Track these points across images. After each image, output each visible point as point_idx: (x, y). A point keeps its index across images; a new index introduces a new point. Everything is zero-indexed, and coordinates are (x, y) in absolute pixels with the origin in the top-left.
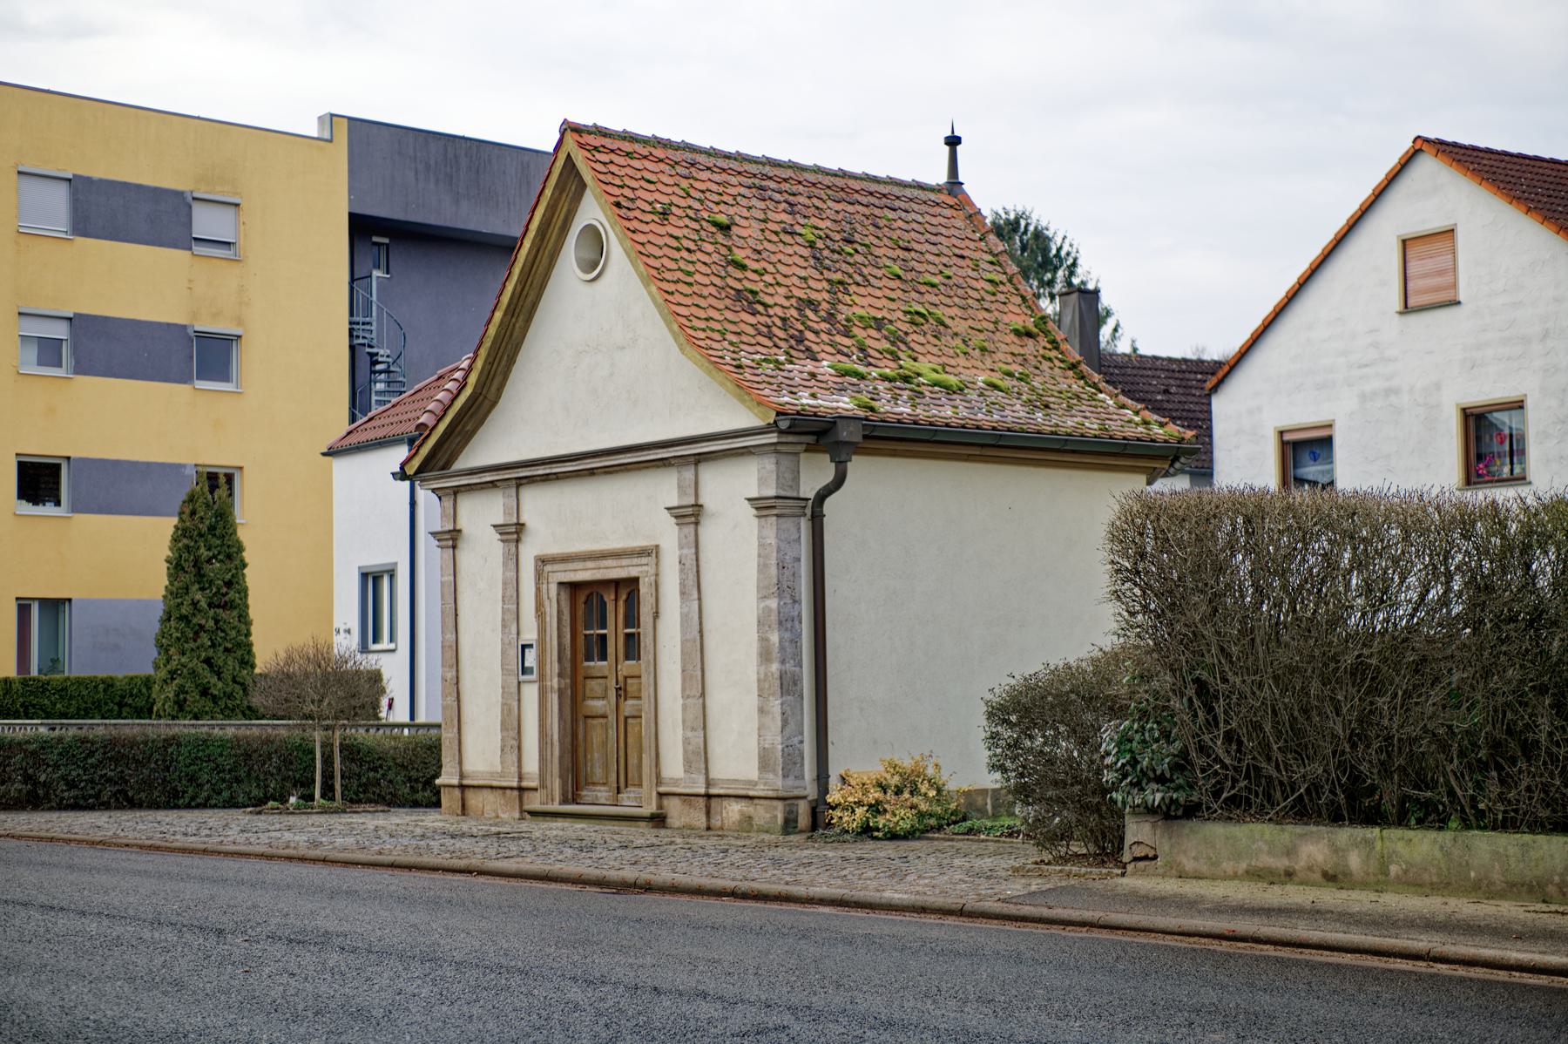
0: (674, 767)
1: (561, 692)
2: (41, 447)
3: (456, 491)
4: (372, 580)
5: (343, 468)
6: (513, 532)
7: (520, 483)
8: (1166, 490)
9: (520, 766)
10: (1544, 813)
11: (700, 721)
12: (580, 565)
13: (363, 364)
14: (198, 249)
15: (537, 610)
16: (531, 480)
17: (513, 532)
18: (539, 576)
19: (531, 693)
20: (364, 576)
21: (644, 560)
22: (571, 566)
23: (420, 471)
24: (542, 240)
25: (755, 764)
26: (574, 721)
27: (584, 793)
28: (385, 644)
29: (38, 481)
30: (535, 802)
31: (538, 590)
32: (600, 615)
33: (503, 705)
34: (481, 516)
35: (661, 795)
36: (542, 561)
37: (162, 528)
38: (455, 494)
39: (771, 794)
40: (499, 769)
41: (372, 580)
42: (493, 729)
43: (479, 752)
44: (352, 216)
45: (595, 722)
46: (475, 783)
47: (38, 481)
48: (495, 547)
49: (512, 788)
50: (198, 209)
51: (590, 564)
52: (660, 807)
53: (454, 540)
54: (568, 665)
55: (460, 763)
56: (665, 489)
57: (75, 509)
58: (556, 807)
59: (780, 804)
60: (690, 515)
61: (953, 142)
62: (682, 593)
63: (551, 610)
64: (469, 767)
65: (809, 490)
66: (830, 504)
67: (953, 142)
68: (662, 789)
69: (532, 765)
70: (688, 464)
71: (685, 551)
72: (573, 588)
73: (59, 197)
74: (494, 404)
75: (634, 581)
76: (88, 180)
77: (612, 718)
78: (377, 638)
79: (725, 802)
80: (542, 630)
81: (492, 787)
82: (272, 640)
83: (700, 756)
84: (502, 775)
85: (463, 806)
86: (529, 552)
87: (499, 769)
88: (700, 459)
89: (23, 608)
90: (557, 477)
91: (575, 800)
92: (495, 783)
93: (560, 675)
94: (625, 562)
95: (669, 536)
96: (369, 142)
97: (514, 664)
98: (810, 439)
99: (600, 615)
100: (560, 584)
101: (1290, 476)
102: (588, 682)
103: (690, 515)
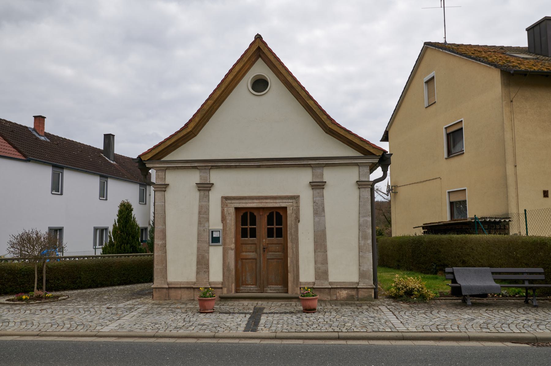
6: (205, 188)
12: (250, 201)
16: (213, 167)
17: (205, 188)
21: (290, 201)
27: (241, 288)
45: (247, 261)
51: (256, 201)
56: (306, 176)
58: (233, 294)
60: (318, 186)
69: (216, 275)
83: (322, 272)
84: (195, 283)
86: (215, 198)
90: (236, 167)
94: (277, 201)
103: (318, 186)
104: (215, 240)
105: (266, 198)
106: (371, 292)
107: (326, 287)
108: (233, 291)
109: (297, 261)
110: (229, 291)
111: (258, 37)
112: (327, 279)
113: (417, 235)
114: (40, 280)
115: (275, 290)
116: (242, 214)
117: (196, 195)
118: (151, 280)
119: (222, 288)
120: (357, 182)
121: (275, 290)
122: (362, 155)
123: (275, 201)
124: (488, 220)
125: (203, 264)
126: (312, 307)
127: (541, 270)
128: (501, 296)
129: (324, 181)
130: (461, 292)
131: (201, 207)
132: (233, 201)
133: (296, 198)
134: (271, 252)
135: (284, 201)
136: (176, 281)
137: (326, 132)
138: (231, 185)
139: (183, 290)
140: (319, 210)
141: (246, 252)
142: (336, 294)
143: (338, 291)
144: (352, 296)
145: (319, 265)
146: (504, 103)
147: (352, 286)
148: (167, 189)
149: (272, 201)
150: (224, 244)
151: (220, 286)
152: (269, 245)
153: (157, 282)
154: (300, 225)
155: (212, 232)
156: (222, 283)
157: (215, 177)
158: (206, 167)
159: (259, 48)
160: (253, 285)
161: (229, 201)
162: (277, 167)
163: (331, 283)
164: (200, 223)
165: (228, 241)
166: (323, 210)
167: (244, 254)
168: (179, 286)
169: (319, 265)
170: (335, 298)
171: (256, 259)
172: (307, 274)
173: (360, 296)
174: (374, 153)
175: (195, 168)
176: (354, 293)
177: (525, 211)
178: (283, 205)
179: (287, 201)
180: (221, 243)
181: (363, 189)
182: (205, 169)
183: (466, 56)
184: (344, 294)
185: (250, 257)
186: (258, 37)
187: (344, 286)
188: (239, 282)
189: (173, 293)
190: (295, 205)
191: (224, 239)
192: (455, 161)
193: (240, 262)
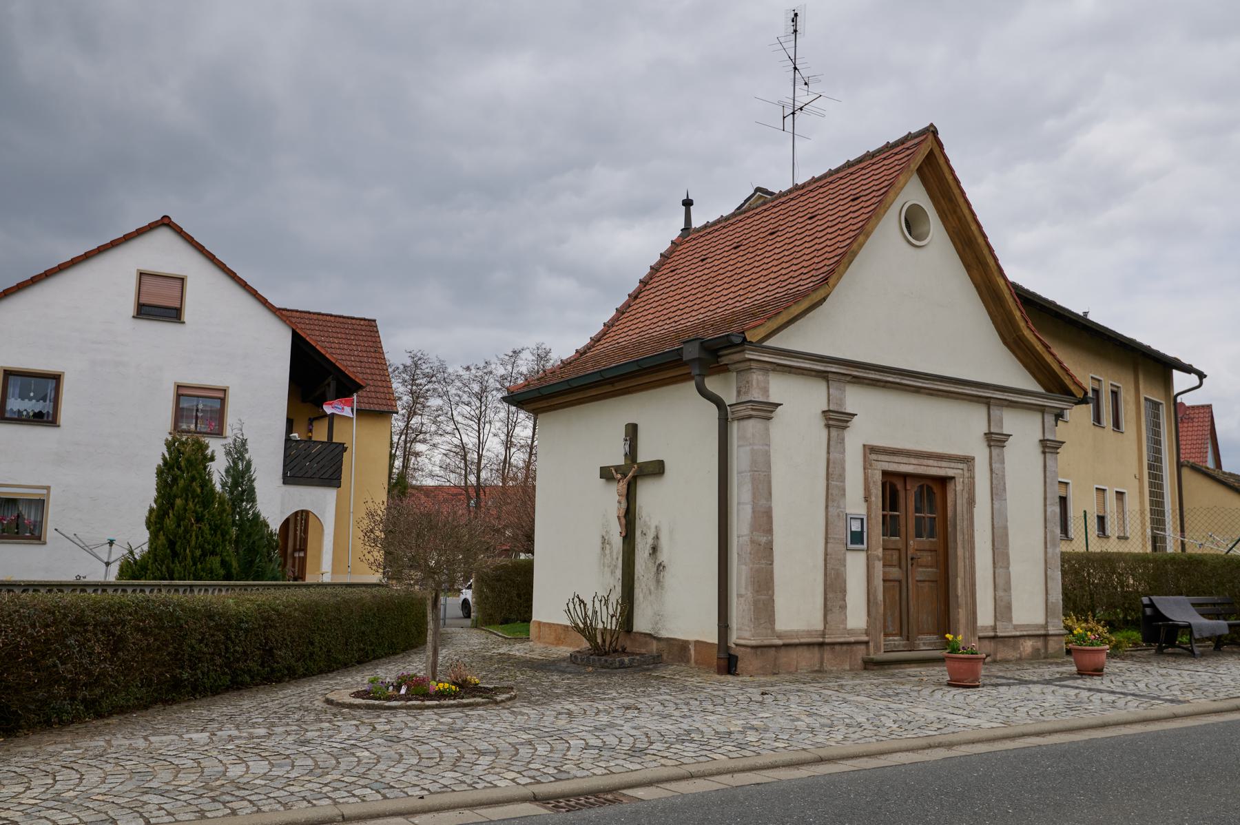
0: (985, 617)
6: (837, 420)
8: (783, 778)
10: (1221, 626)
11: (1002, 585)
12: (905, 460)
16: (857, 381)
17: (837, 420)
21: (961, 466)
22: (896, 459)
51: (913, 461)
59: (735, 428)
60: (995, 440)
69: (856, 617)
79: (1021, 641)
83: (1003, 609)
90: (918, 390)
94: (944, 464)
95: (981, 454)
101: (1155, 548)
103: (995, 440)
104: (857, 538)
109: (973, 585)
112: (1010, 619)
113: (1189, 550)
115: (930, 644)
119: (867, 643)
120: (824, 412)
121: (930, 644)
122: (1042, 391)
123: (940, 464)
125: (834, 588)
129: (773, 399)
130: (530, 607)
133: (968, 461)
134: (921, 566)
135: (953, 465)
136: (789, 629)
137: (1005, 343)
138: (883, 421)
139: (800, 649)
140: (997, 491)
151: (865, 638)
156: (867, 633)
157: (855, 399)
158: (843, 378)
161: (874, 457)
162: (948, 397)
163: (1016, 627)
166: (1005, 489)
168: (796, 641)
171: (900, 581)
173: (1050, 651)
178: (950, 473)
182: (839, 381)
184: (1028, 646)
189: (786, 657)
190: (967, 475)
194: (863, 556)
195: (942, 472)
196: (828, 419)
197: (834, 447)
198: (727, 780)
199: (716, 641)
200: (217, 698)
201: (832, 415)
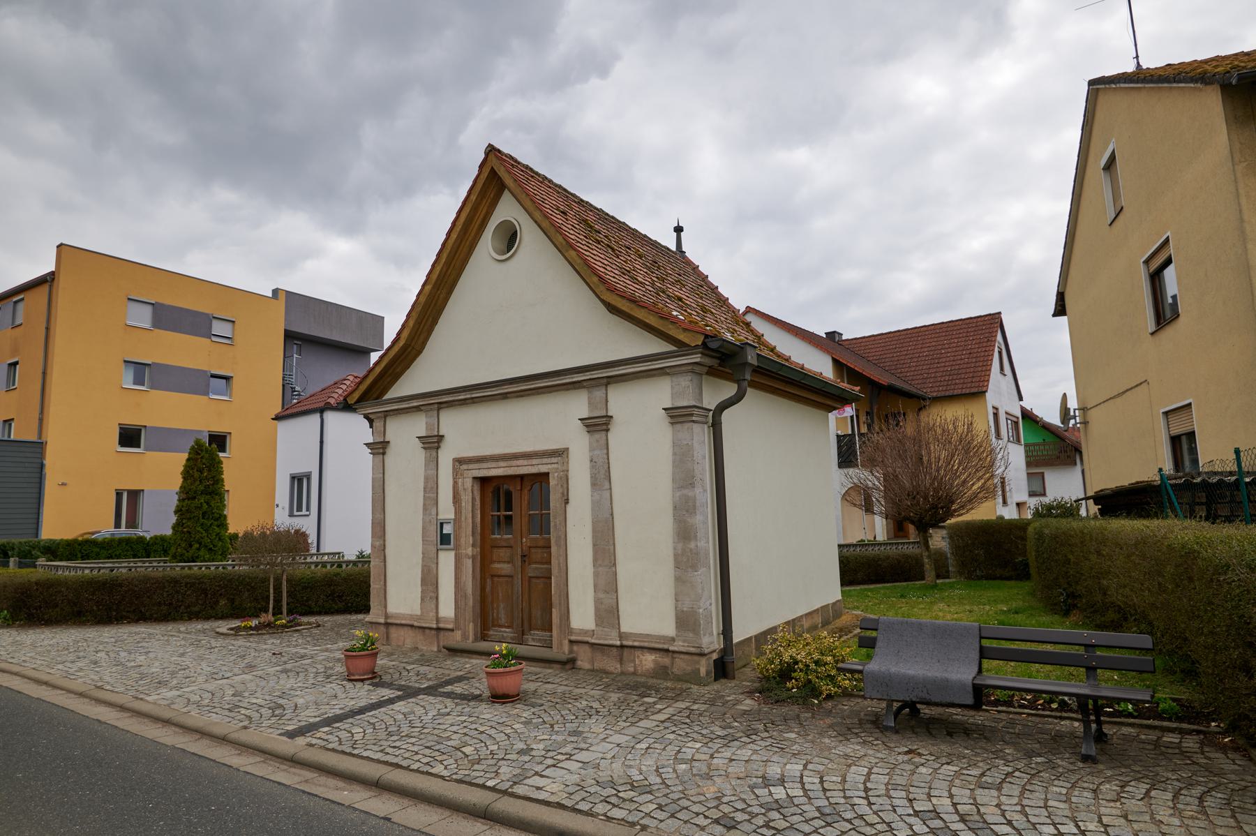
1: (474, 558)
2: (132, 420)
3: (386, 414)
4: (298, 481)
5: (284, 428)
6: (432, 442)
7: (441, 406)
9: (437, 612)
10: (1168, 694)
11: (607, 585)
12: (494, 464)
13: (288, 388)
14: (214, 339)
15: (454, 497)
16: (450, 404)
17: (432, 442)
18: (456, 474)
19: (447, 560)
20: (293, 478)
21: (554, 460)
23: (358, 401)
24: (465, 234)
25: (673, 625)
26: (483, 579)
27: (491, 633)
28: (304, 512)
29: (130, 437)
30: (456, 639)
31: (455, 483)
32: (513, 505)
33: (423, 566)
34: (405, 433)
35: (571, 642)
36: (459, 461)
37: (183, 457)
38: (385, 417)
39: (692, 650)
40: (419, 613)
41: (298, 481)
42: (419, 586)
43: (400, 596)
44: (286, 331)
45: (501, 579)
46: (398, 622)
47: (130, 437)
48: (419, 455)
49: (431, 629)
50: (215, 323)
51: (502, 464)
52: (571, 652)
53: (384, 448)
54: (478, 537)
55: (386, 607)
56: (578, 406)
57: (146, 449)
58: (470, 644)
60: (598, 425)
61: (679, 230)
62: (594, 485)
63: (466, 499)
64: (392, 609)
65: (710, 401)
66: (726, 415)
67: (679, 230)
68: (573, 638)
69: (447, 609)
70: (601, 385)
71: (597, 452)
72: (483, 481)
73: (147, 312)
74: (419, 352)
75: (547, 474)
76: (162, 305)
77: (518, 581)
78: (299, 509)
80: (458, 511)
81: (412, 626)
82: (240, 518)
83: (608, 613)
84: (419, 618)
85: (388, 638)
86: (446, 457)
87: (419, 613)
88: (610, 381)
89: (119, 494)
90: (473, 401)
91: (484, 637)
92: (416, 624)
93: (473, 545)
94: (535, 462)
95: (580, 447)
96: (295, 302)
97: (434, 537)
98: (715, 362)
99: (513, 505)
100: (474, 478)
102: (495, 550)
103: (598, 425)
105: (515, 457)
106: (698, 663)
107: (611, 642)
108: (471, 637)
110: (465, 636)
111: (491, 151)
114: (278, 601)
116: (491, 489)
117: (367, 457)
118: (366, 609)
124: (1214, 480)
126: (512, 691)
127: (1146, 641)
128: (1054, 706)
131: (427, 479)
132: (471, 466)
133: (561, 453)
135: (545, 461)
140: (601, 477)
141: (499, 562)
142: (634, 661)
143: (638, 653)
144: (665, 668)
145: (602, 596)
146: (1239, 168)
147: (660, 646)
148: (442, 445)
149: (525, 462)
150: (457, 548)
151: (450, 626)
152: (533, 550)
153: (375, 615)
154: (569, 508)
155: (442, 524)
159: (493, 172)
160: (508, 627)
161: (465, 467)
162: (638, 378)
164: (425, 509)
165: (463, 540)
167: (496, 565)
169: (602, 596)
170: (632, 669)
172: (582, 615)
174: (686, 340)
175: (418, 409)
176: (666, 661)
177: (1237, 452)
178: (543, 469)
179: (548, 460)
180: (452, 546)
181: (678, 426)
183: (1152, 81)
184: (648, 661)
185: (503, 573)
186: (491, 151)
187: (646, 644)
188: (485, 623)
191: (457, 539)
192: (1169, 332)
193: (489, 581)
194: (452, 554)
195: (534, 470)
196: (671, 417)
197: (433, 463)
198: (940, 710)
199: (452, 615)
200: (30, 626)
201: (676, 412)
